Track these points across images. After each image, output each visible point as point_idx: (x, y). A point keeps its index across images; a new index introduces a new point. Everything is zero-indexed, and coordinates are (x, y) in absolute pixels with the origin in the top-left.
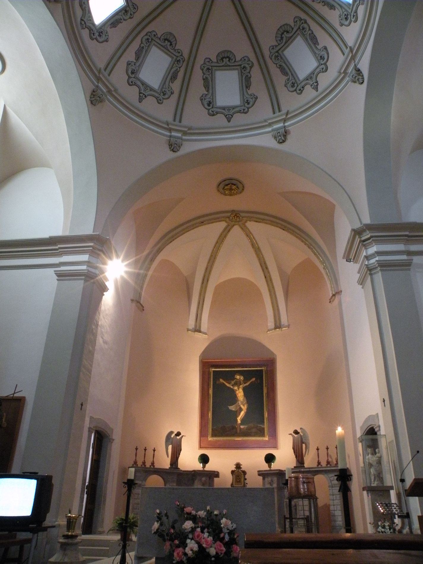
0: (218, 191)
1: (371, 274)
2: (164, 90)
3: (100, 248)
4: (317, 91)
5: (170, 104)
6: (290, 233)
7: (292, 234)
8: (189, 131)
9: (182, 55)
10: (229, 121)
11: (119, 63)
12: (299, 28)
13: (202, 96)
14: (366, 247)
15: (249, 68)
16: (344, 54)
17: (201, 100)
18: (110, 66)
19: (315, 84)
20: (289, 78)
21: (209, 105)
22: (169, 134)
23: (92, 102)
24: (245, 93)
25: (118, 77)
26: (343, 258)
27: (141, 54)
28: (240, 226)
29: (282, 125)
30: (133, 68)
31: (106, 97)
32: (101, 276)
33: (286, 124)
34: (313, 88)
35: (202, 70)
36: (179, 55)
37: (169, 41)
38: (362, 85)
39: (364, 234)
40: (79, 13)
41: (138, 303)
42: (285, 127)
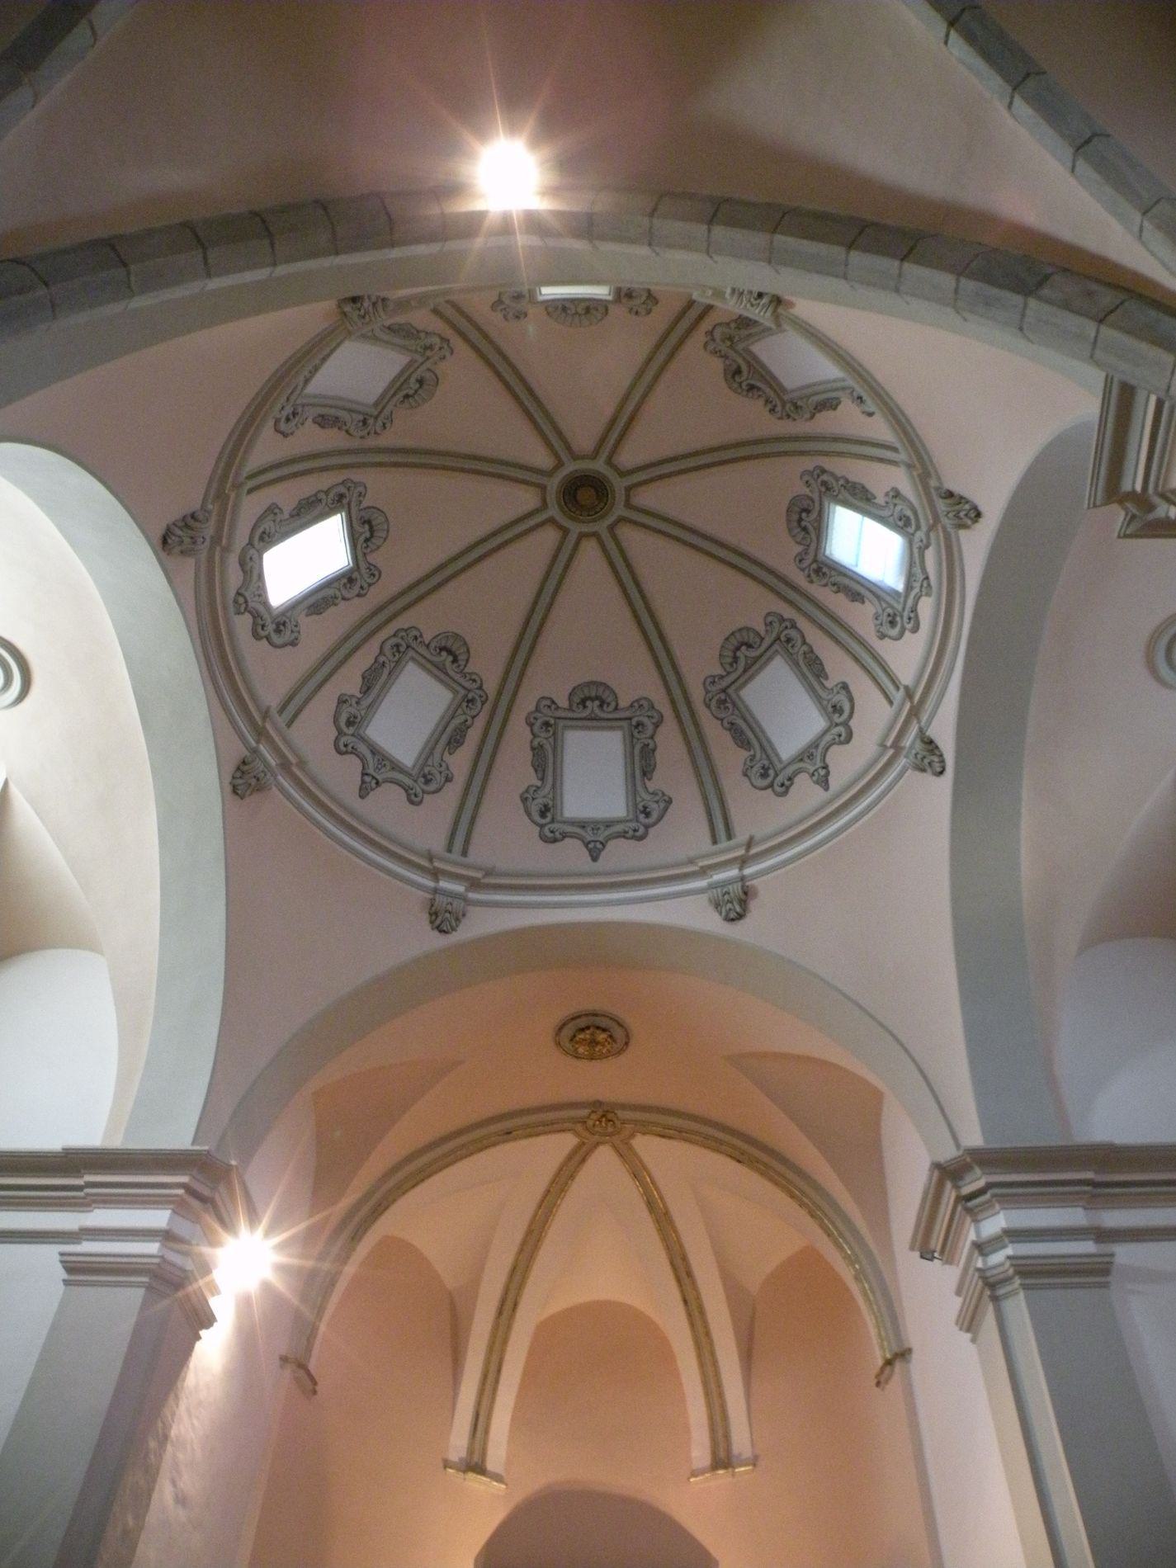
0: (558, 1044)
1: (995, 1299)
2: (426, 770)
3: (206, 1192)
4: (827, 789)
5: (445, 803)
6: (757, 1170)
7: (762, 1174)
8: (486, 881)
9: (480, 688)
10: (595, 859)
11: (316, 698)
12: (778, 638)
13: (527, 791)
14: (975, 1215)
15: (650, 728)
16: (891, 703)
17: (524, 800)
18: (294, 704)
19: (823, 772)
20: (754, 756)
21: (543, 814)
22: (431, 884)
23: (235, 791)
24: (640, 788)
25: (313, 733)
26: (912, 1248)
27: (374, 681)
28: (614, 1147)
29: (733, 872)
30: (353, 710)
31: (274, 776)
32: (201, 1282)
33: (747, 871)
34: (817, 783)
35: (531, 725)
36: (475, 686)
37: (449, 652)
38: (942, 777)
39: (968, 1178)
40: (234, 578)
41: (299, 1366)
42: (743, 879)
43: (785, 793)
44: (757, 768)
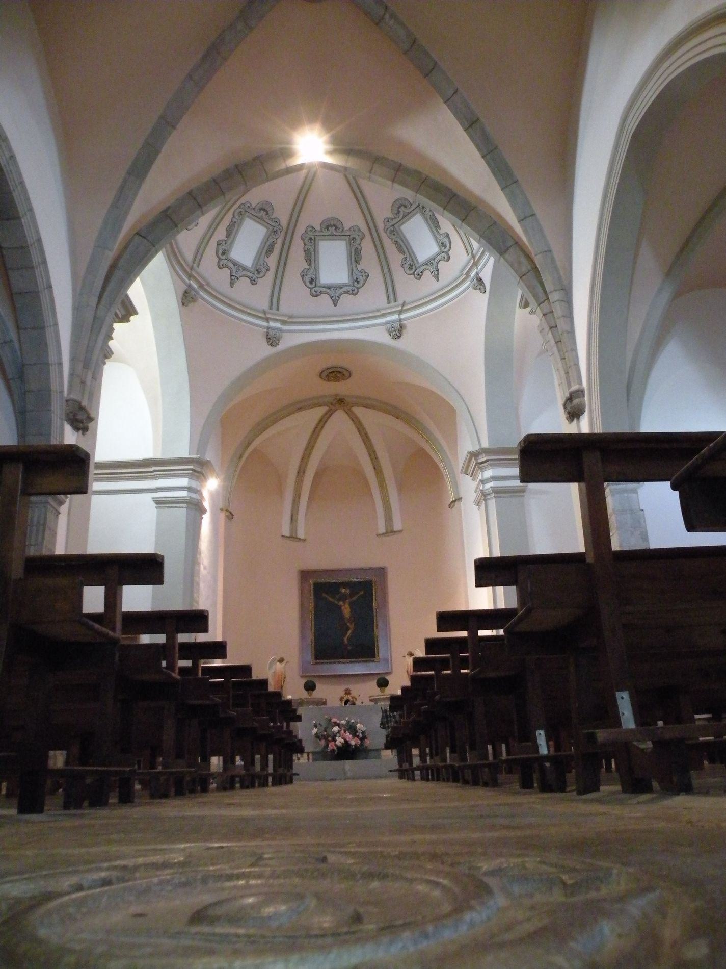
1: (485, 500)
14: (482, 470)
17: (302, 276)
18: (198, 254)
21: (311, 283)
25: (208, 266)
29: (396, 317)
33: (403, 316)
37: (264, 210)
42: (400, 320)
43: (420, 279)
44: (407, 265)
